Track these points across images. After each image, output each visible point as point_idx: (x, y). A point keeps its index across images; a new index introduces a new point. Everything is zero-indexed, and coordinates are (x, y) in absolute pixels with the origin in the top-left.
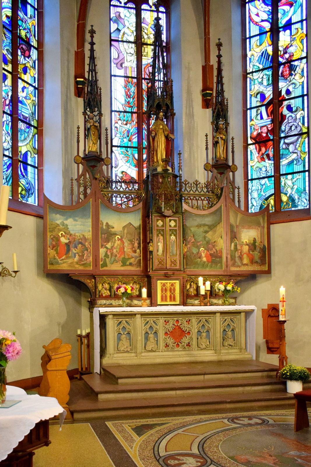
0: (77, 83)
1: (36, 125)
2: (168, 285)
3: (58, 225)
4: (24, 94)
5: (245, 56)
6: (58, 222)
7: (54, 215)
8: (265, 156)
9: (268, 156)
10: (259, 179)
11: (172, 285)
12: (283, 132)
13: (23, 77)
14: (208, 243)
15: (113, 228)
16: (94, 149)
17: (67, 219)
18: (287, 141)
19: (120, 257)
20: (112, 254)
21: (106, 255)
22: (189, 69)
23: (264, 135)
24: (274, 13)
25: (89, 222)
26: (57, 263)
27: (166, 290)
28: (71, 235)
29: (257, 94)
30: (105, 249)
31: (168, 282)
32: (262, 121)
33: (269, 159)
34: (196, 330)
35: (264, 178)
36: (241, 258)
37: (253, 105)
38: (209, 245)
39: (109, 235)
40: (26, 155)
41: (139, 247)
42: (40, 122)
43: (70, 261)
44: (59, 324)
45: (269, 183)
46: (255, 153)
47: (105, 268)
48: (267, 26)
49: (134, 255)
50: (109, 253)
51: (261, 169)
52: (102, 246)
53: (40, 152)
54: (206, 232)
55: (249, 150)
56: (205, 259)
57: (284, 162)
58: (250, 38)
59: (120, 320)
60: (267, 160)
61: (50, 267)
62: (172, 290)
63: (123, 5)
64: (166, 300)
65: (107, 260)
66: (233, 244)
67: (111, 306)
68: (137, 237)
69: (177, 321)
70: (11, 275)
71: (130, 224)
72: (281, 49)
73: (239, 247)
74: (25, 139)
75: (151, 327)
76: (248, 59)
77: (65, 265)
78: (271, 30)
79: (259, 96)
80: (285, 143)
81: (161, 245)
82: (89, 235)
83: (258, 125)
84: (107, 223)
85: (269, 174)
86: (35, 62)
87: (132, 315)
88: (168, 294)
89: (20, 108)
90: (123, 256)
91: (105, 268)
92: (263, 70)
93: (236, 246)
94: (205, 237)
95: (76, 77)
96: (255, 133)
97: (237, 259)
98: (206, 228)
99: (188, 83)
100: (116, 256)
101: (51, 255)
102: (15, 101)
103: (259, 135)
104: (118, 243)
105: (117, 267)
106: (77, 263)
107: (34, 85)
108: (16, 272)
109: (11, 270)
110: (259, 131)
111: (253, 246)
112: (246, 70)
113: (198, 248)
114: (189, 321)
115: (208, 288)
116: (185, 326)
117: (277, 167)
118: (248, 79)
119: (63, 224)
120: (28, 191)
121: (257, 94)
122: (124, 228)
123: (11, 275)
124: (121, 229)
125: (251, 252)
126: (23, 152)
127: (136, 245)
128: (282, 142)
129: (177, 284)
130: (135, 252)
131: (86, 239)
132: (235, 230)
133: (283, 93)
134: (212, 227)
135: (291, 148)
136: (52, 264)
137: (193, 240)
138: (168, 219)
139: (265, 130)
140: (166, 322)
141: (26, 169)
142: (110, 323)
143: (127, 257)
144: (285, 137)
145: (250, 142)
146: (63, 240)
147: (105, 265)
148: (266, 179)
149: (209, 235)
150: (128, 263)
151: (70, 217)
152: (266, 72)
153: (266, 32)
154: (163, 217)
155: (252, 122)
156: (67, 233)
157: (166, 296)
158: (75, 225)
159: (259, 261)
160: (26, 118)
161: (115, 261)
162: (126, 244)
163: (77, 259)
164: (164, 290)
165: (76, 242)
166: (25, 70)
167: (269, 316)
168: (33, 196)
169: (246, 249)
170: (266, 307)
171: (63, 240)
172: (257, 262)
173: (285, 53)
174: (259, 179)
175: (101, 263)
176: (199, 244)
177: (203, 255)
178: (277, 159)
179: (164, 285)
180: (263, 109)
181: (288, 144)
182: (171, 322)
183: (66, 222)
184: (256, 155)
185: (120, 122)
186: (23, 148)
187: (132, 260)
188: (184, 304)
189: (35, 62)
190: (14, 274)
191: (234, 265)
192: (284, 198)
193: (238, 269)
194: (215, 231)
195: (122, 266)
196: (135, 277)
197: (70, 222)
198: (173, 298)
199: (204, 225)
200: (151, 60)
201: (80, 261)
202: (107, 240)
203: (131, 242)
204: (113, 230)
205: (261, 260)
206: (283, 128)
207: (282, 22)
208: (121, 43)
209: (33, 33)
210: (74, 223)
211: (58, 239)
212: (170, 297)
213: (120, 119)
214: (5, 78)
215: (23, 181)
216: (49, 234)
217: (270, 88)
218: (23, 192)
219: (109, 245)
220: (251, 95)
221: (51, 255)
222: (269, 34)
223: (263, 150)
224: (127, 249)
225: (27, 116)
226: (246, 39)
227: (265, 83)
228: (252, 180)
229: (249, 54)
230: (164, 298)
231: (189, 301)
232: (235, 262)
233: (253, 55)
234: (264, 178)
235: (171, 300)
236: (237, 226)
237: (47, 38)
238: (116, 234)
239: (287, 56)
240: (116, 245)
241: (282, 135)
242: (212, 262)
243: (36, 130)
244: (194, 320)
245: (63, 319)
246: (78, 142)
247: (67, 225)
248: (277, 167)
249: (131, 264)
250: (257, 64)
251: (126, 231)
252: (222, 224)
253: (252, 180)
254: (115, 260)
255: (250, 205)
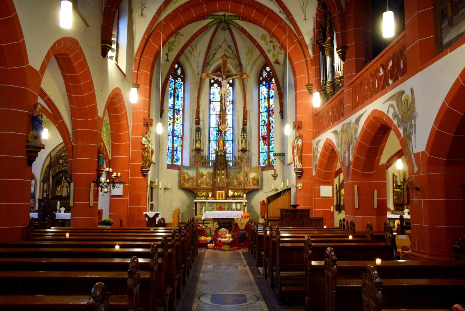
0: (196, 121)
1: (264, 71)
2: (221, 193)
3: (185, 173)
4: (177, 128)
5: (259, 106)
6: (185, 172)
7: (184, 169)
8: (265, 144)
9: (266, 144)
10: (263, 152)
11: (222, 193)
12: (271, 136)
13: (177, 122)
14: (237, 178)
15: (203, 173)
16: (198, 147)
17: (188, 171)
18: (272, 139)
19: (205, 183)
20: (203, 182)
21: (201, 183)
22: (238, 112)
23: (265, 136)
24: (269, 91)
25: (195, 172)
26: (184, 185)
27: (220, 195)
28: (189, 176)
29: (263, 121)
30: (200, 181)
31: (221, 192)
32: (264, 131)
33: (266, 145)
34: (227, 208)
35: (265, 152)
36: (249, 183)
37: (262, 125)
38: (237, 179)
39: (202, 176)
40: (177, 148)
41: (212, 180)
42: (183, 136)
43: (188, 184)
44: (186, 205)
45: (266, 154)
46: (262, 142)
47: (200, 187)
48: (267, 96)
49: (210, 182)
50: (202, 182)
51: (264, 149)
52: (199, 180)
53: (182, 146)
54: (236, 174)
55: (260, 141)
56: (236, 184)
57: (271, 147)
58: (261, 99)
59: (201, 204)
60: (266, 146)
61: (182, 186)
62: (222, 195)
63: (216, 88)
64: (220, 198)
65: (201, 184)
66: (246, 179)
67: (201, 199)
68: (211, 176)
69: (221, 205)
70: (168, 189)
71: (209, 172)
72: (270, 105)
73: (248, 179)
74: (177, 143)
75: (229, 207)
76: (261, 107)
77: (187, 186)
78: (267, 98)
79: (264, 121)
80: (271, 140)
81: (219, 179)
82: (195, 176)
83: (157, 180)
84: (201, 172)
85: (266, 151)
86: (181, 116)
87: (205, 203)
88: (221, 196)
89: (175, 133)
90: (206, 183)
91: (200, 187)
92: (265, 112)
93: (247, 179)
94: (236, 176)
95: (196, 119)
96: (262, 135)
97: (248, 184)
98: (237, 173)
99: (238, 117)
100: (204, 183)
101: (183, 183)
102: (173, 130)
103: (264, 136)
104: (205, 178)
105: (204, 186)
106: (191, 185)
107: (181, 123)
108: (169, 189)
109: (168, 188)
110: (264, 135)
111: (254, 179)
112: (260, 111)
113: (233, 180)
114: (224, 205)
115: (232, 194)
116: (223, 207)
117: (269, 148)
118: (261, 115)
119: (187, 172)
120: (177, 160)
121: (263, 121)
122: (207, 173)
123: (168, 189)
124: (206, 174)
125: (253, 181)
126: (176, 147)
127: (211, 179)
128: (270, 139)
129: (224, 192)
130: (211, 181)
131: (194, 177)
132: (247, 173)
133: (271, 121)
134: (239, 173)
135: (273, 142)
136: (183, 185)
137: (231, 177)
138: (221, 171)
139: (265, 134)
140: (217, 205)
141: (177, 153)
142: (198, 205)
143: (208, 183)
144: (271, 138)
145: (261, 138)
146: (187, 178)
147: (200, 186)
148: (265, 153)
149: (238, 175)
150: (208, 185)
151: (189, 170)
152: (266, 113)
153: (266, 98)
154: (219, 170)
155: (262, 131)
156: (188, 175)
157: (220, 197)
158: (191, 173)
159: (256, 184)
160: (177, 135)
161: (204, 184)
162: (208, 179)
163: (191, 183)
164: (219, 194)
165: (191, 178)
166: (177, 120)
167: (263, 205)
168: (179, 161)
169: (251, 180)
170: (261, 201)
171: (187, 178)
172: (255, 185)
173: (272, 107)
174: (263, 152)
175: (199, 185)
176: (233, 178)
177: (235, 182)
178: (269, 145)
179: (219, 193)
180: (265, 126)
181: (272, 141)
182: (218, 205)
183: (188, 172)
184: (263, 143)
185: (213, 131)
186: (176, 145)
187: (209, 184)
188: (226, 199)
189: (181, 116)
190: (169, 189)
191: (246, 186)
192: (271, 161)
193: (248, 187)
194: (240, 174)
195: (206, 186)
196: (210, 190)
197: (189, 172)
198: (222, 197)
199: (236, 172)
200: (227, 109)
201: (192, 184)
202: (201, 177)
203: (209, 178)
204: (203, 174)
205: (257, 184)
206: (271, 134)
207: (271, 96)
208: (215, 102)
209: (181, 106)
210: (190, 172)
211: (184, 177)
212: (221, 197)
213: (213, 130)
214: (170, 124)
215: (175, 157)
216: (182, 176)
217: (267, 119)
218: (176, 161)
219: (202, 179)
220: (261, 121)
221: (183, 183)
222: (267, 99)
223: (265, 141)
224: (208, 180)
225: (178, 135)
226: (260, 100)
227: (266, 117)
228: (261, 153)
229: (261, 105)
230: (219, 197)
231: (228, 198)
232: (247, 185)
233: (262, 106)
234: (265, 152)
235: (221, 198)
236: (248, 172)
237: (186, 107)
238: (204, 175)
239: (272, 108)
240: (204, 179)
241: (270, 137)
242: (239, 184)
243: (181, 139)
244: (226, 205)
245: (188, 204)
246: (193, 144)
247: (188, 173)
248: (269, 148)
249: (209, 185)
250: (263, 109)
251: (208, 174)
252: (242, 171)
253: (261, 153)
254: (204, 184)
255: (261, 162)
